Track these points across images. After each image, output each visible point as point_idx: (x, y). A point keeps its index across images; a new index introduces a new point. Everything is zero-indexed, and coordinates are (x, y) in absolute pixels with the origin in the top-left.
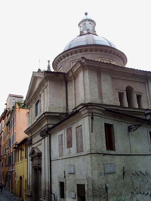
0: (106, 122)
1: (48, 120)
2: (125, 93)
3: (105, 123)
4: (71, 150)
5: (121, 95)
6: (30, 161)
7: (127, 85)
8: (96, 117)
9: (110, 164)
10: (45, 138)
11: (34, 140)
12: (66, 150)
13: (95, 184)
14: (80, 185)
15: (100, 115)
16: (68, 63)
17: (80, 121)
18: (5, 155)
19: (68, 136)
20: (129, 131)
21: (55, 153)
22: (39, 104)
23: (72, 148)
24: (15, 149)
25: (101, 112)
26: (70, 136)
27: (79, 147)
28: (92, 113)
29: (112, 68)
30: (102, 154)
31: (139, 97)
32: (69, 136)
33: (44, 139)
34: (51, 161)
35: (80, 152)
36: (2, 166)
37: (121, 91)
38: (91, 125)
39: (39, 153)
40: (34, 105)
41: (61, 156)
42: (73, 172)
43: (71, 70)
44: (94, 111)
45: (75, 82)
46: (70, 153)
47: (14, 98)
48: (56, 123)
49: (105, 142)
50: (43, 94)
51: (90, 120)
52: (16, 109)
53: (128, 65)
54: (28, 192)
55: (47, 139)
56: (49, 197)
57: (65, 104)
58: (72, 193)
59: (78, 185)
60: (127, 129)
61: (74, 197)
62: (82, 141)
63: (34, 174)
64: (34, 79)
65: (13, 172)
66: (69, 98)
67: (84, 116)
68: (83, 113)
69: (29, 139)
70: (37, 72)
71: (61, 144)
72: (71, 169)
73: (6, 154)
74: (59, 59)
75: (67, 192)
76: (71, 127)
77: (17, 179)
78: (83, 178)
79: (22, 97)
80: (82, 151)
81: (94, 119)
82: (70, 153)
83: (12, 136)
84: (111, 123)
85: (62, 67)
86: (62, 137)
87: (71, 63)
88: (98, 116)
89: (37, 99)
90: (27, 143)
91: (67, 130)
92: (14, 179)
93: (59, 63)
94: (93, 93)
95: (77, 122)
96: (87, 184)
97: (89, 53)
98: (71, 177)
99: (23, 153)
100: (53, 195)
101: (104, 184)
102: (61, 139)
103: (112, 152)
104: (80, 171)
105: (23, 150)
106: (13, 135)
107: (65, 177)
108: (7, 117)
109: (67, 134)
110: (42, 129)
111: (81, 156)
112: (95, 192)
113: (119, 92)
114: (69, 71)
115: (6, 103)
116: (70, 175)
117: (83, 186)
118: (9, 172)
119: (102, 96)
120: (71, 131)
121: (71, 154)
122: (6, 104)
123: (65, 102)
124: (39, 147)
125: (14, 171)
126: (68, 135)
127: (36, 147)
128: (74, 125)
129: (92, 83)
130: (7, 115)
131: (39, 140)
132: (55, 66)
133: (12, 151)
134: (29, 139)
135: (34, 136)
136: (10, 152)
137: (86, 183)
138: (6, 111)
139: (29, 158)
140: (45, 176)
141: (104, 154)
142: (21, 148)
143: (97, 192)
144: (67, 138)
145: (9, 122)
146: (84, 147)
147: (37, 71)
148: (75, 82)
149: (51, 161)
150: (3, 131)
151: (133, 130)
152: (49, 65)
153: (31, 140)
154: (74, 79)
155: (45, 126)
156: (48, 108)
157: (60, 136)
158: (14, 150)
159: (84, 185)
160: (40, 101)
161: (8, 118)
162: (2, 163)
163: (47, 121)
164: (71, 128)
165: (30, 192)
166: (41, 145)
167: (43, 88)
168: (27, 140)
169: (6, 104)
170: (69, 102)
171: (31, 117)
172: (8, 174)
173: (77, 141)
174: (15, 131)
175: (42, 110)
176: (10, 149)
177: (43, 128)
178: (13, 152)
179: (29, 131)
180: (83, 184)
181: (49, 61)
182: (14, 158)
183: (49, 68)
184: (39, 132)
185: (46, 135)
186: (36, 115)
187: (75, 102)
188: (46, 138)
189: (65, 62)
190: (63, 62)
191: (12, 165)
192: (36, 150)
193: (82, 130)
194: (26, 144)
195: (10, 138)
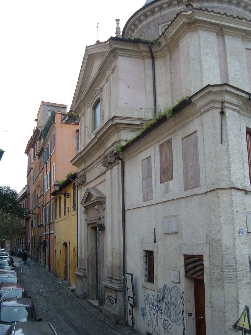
3: (246, 127)
6: (83, 215)
8: (231, 111)
11: (90, 177)
13: (229, 255)
14: (193, 256)
15: (237, 108)
16: (153, 29)
17: (191, 124)
18: (37, 208)
19: (164, 159)
21: (135, 194)
22: (98, 109)
23: (171, 183)
24: (54, 196)
25: (240, 103)
26: (169, 157)
27: (190, 178)
28: (222, 103)
32: (166, 158)
33: (110, 171)
34: (124, 211)
35: (192, 188)
36: (32, 227)
38: (220, 128)
39: (101, 198)
40: (89, 111)
41: (148, 200)
42: (175, 230)
43: (163, 33)
44: (227, 98)
45: (171, 60)
46: (167, 191)
49: (247, 165)
50: (107, 85)
52: (54, 124)
54: (79, 270)
55: (116, 169)
56: (121, 280)
57: (152, 103)
58: (172, 272)
59: (186, 257)
61: (177, 281)
62: (197, 165)
63: (89, 235)
64: (90, 56)
65: (51, 235)
66: (158, 90)
67: (202, 111)
68: (199, 104)
69: (81, 174)
70: (95, 45)
71: (147, 176)
72: (169, 225)
73: (38, 206)
74: (135, 20)
76: (171, 139)
77: (59, 247)
78: (198, 243)
79: (64, 107)
80: (198, 186)
82: (167, 191)
83: (48, 173)
88: (234, 110)
89: (96, 96)
90: (77, 182)
91: (162, 146)
92: (54, 247)
93: (136, 31)
94: (210, 77)
95: (184, 126)
96: (208, 253)
98: (170, 239)
99: (70, 202)
100: (128, 277)
101: (247, 256)
104: (192, 228)
105: (68, 195)
106: (50, 171)
107: (155, 241)
108: (38, 142)
109: (161, 154)
110: (105, 151)
111: (195, 197)
112: (228, 270)
114: (159, 37)
115: (37, 118)
116: (168, 237)
117: (200, 258)
118: (44, 236)
121: (170, 193)
122: (36, 120)
124: (99, 187)
125: (53, 233)
126: (164, 156)
127: (94, 188)
128: (178, 133)
129: (207, 57)
130: (39, 137)
131: (101, 173)
133: (48, 200)
134: (81, 174)
135: (90, 168)
136: (45, 202)
137: (205, 252)
138: (36, 132)
139: (81, 209)
140: (111, 241)
142: (66, 192)
143: (231, 271)
144: (161, 163)
145: (42, 150)
148: (171, 60)
149: (124, 211)
150: (32, 169)
153: (84, 176)
155: (113, 145)
157: (145, 161)
158: (52, 197)
159: (201, 257)
161: (40, 143)
162: (32, 222)
163: (168, 55)
164: (169, 142)
165: (83, 271)
166: (105, 183)
167: (107, 74)
168: (77, 177)
169: (36, 120)
170: (158, 99)
172: (43, 240)
173: (186, 165)
174: (54, 164)
176: (45, 196)
177: (107, 149)
178: (50, 202)
179: (77, 162)
180: (200, 255)
181: (118, 20)
182: (53, 212)
184: (101, 159)
186: (94, 128)
190: (143, 27)
191: (50, 224)
192: (93, 192)
195: (45, 177)
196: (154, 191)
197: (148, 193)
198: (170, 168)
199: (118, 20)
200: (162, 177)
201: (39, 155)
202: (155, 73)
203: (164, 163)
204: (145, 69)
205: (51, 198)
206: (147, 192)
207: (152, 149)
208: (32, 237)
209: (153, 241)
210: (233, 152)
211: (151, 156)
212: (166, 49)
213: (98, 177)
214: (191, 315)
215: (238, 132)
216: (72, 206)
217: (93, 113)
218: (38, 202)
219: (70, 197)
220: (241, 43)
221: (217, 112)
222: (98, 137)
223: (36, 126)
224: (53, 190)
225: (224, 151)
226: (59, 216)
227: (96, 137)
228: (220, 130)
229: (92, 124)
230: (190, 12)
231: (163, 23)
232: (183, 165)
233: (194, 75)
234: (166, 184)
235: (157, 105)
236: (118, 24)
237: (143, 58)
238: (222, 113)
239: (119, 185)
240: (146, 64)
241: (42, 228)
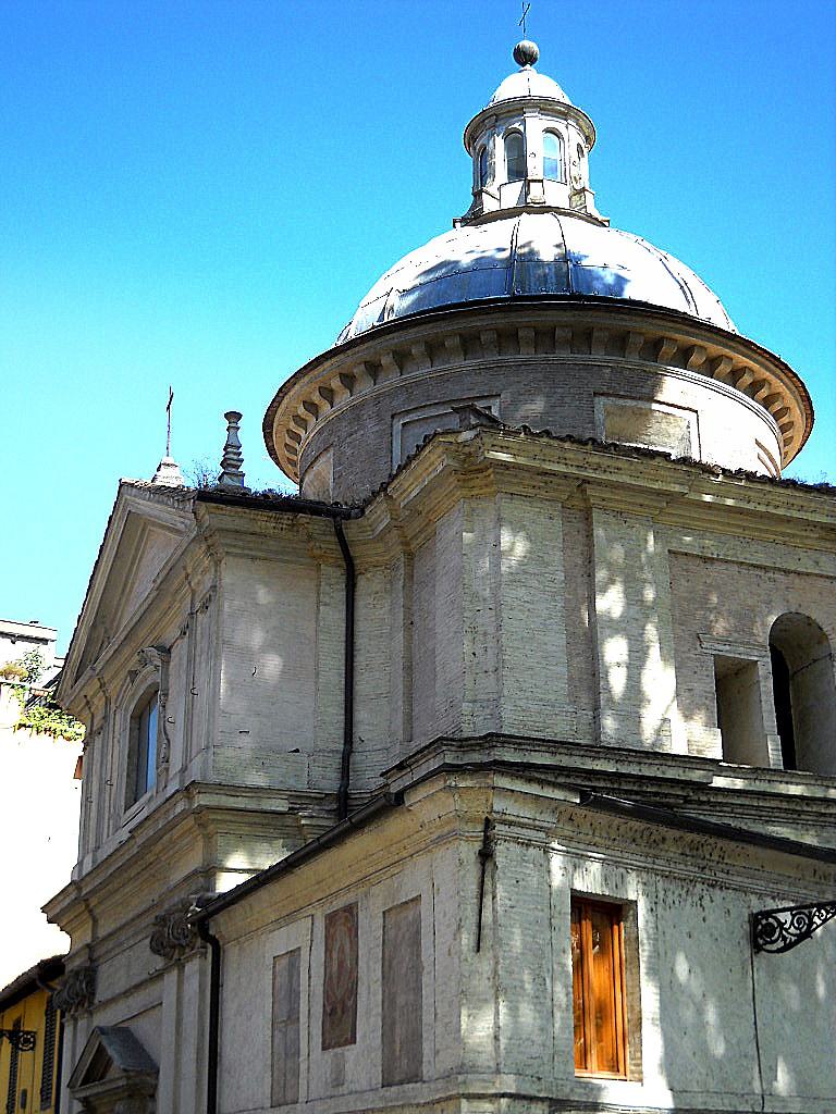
2: (765, 668)
4: (349, 1066)
10: (181, 968)
11: (111, 979)
12: (315, 1062)
16: (371, 427)
19: (335, 968)
20: (757, 949)
23: (351, 1052)
25: (548, 819)
28: (488, 824)
29: (677, 488)
30: (542, 1100)
32: (341, 964)
35: (401, 1083)
48: (266, 862)
55: (196, 970)
57: (338, 731)
60: (742, 929)
64: (134, 512)
66: (362, 686)
71: (285, 1019)
80: (415, 1077)
81: (500, 859)
86: (293, 968)
87: (398, 425)
91: (331, 919)
94: (530, 662)
97: (526, 363)
102: (291, 976)
105: (27, 1041)
120: (353, 932)
126: (335, 956)
131: (145, 976)
142: (17, 1023)
146: (427, 1048)
151: (781, 944)
154: (204, 836)
160: (166, 695)
170: (361, 714)
171: (94, 807)
173: (389, 1001)
175: (176, 763)
183: (232, 459)
186: (134, 796)
187: (409, 719)
188: (193, 967)
189: (358, 418)
193: (418, 932)
194: (50, 1002)
197: (289, 1077)
198: (350, 1003)
199: (233, 417)
200: (328, 1025)
202: (356, 618)
203: (335, 981)
204: (318, 603)
206: (285, 1076)
210: (514, 979)
211: (299, 948)
213: (137, 987)
215: (537, 913)
216: (40, 1086)
217: (136, 733)
219: (32, 1049)
221: (469, 851)
222: (140, 841)
225: (485, 976)
228: (477, 911)
229: (128, 775)
230: (467, 435)
231: (408, 412)
232: (383, 1002)
233: (474, 654)
234: (336, 1055)
235: (356, 740)
237: (316, 562)
238: (486, 856)
239: (201, 1035)
240: (324, 588)
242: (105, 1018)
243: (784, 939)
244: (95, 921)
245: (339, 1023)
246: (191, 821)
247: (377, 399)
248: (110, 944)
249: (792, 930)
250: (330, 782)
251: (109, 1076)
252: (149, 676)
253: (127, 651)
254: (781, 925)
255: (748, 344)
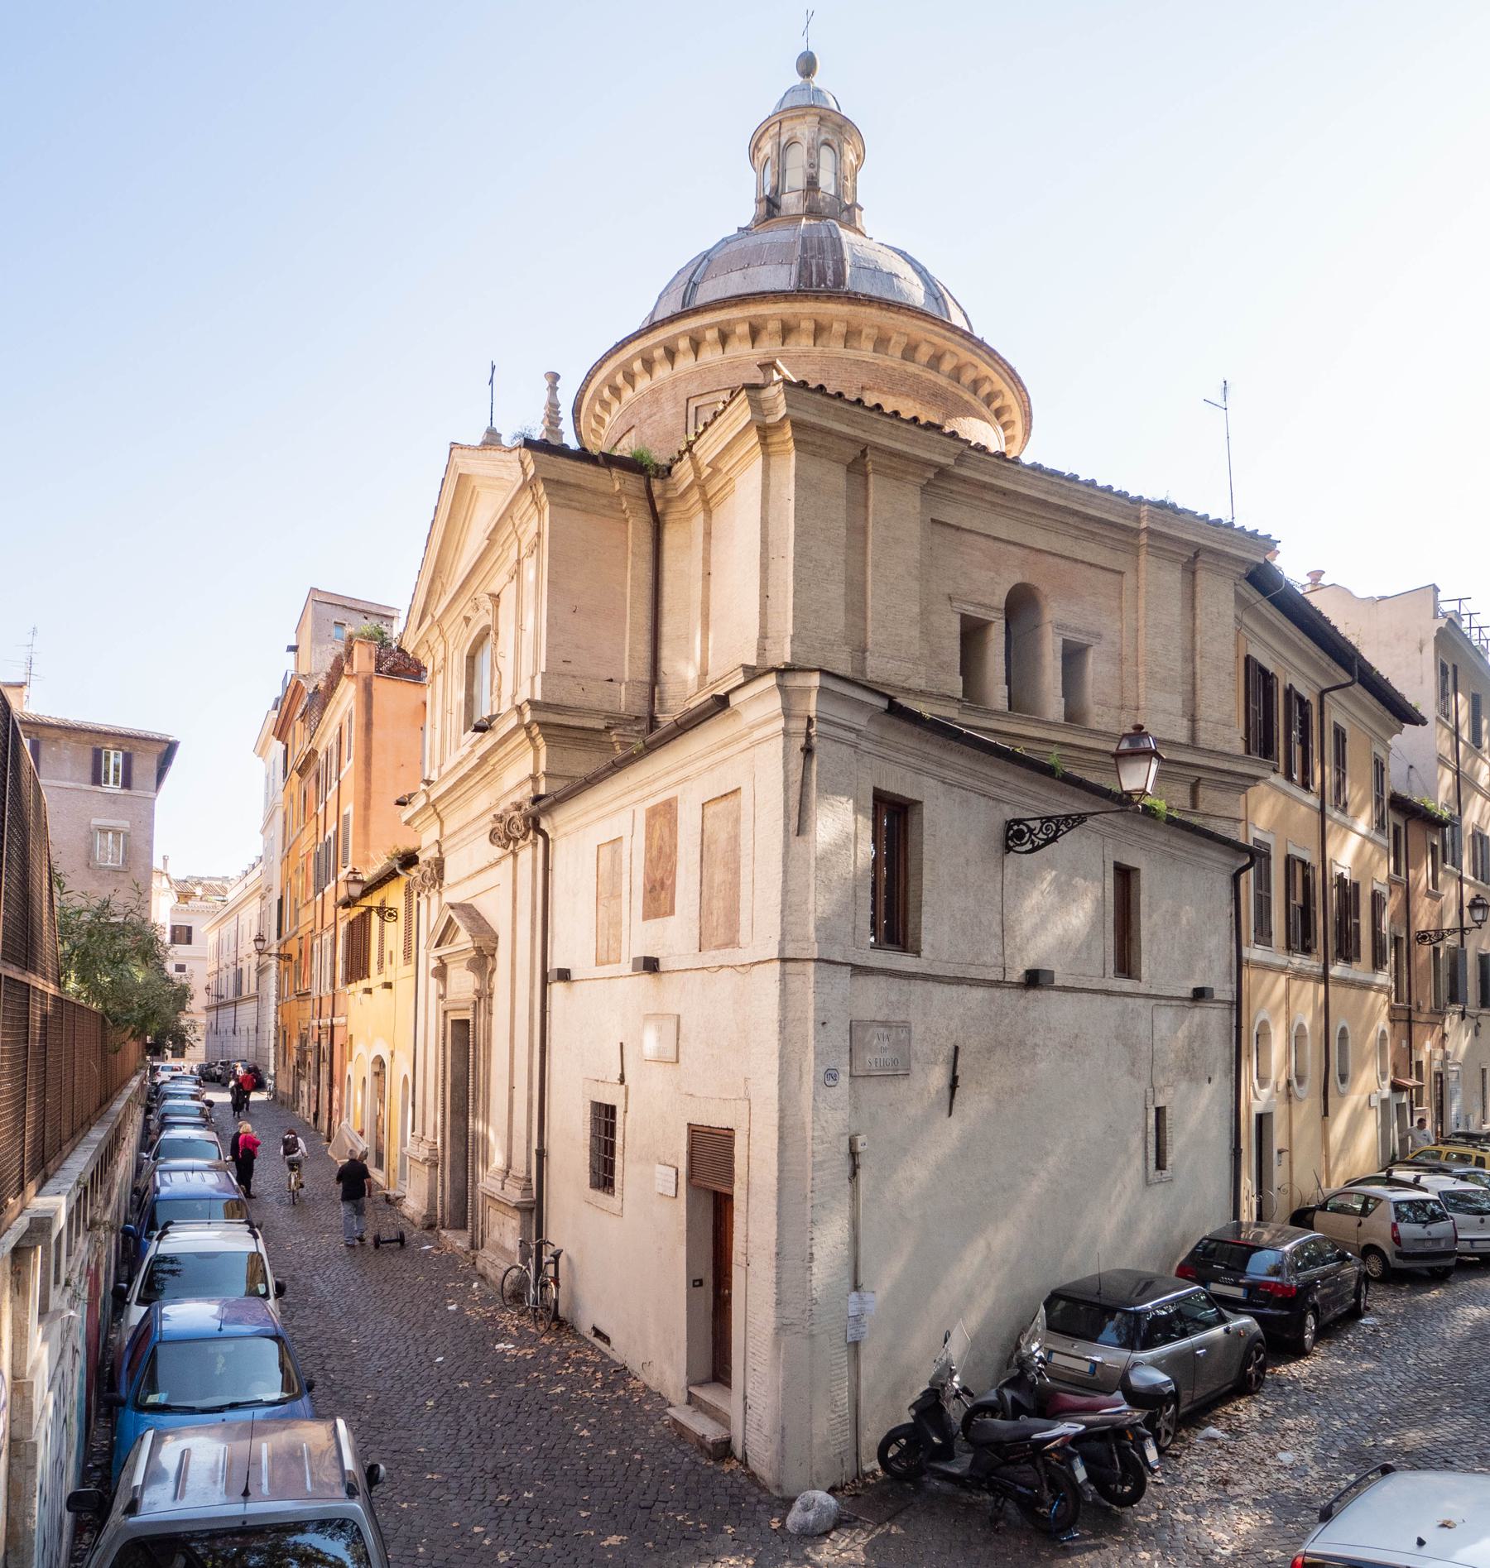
0: (893, 786)
1: (536, 749)
5: (972, 633)
6: (433, 981)
7: (1017, 578)
9: (885, 1024)
10: (515, 854)
14: (711, 1131)
15: (853, 736)
23: (670, 921)
25: (860, 721)
26: (667, 850)
31: (1073, 656)
37: (980, 613)
47: (339, 615)
51: (797, 758)
53: (1043, 449)
55: (527, 854)
60: (998, 831)
71: (607, 891)
74: (612, 375)
75: (626, 1168)
80: (732, 942)
84: (909, 793)
85: (633, 432)
103: (905, 962)
107: (622, 1080)
108: (298, 724)
109: (649, 837)
113: (965, 618)
117: (725, 1137)
119: (609, 1167)
123: (644, 650)
132: (594, 424)
141: (859, 970)
147: (477, 443)
151: (1029, 846)
152: (553, 407)
156: (538, 679)
181: (555, 377)
183: (553, 418)
185: (524, 837)
188: (526, 855)
189: (657, 401)
194: (408, 887)
196: (625, 938)
198: (668, 882)
201: (302, 771)
205: (340, 916)
207: (626, 815)
208: (277, 1028)
209: (616, 1078)
212: (695, 495)
214: (701, 1284)
218: (297, 923)
220: (918, 505)
223: (292, 667)
224: (342, 894)
226: (701, 539)
227: (472, 751)
236: (553, 389)
241: (310, 1004)
242: (453, 896)
243: (1033, 842)
244: (442, 822)
245: (658, 897)
246: (522, 734)
247: (675, 383)
248: (455, 840)
249: (1041, 836)
250: (640, 707)
251: (457, 941)
252: (482, 620)
253: (462, 601)
254: (1031, 831)
255: (992, 353)
